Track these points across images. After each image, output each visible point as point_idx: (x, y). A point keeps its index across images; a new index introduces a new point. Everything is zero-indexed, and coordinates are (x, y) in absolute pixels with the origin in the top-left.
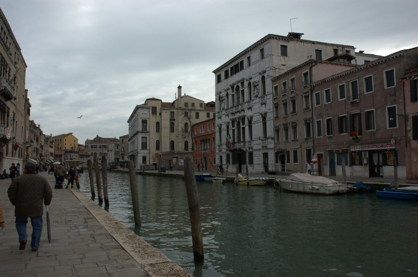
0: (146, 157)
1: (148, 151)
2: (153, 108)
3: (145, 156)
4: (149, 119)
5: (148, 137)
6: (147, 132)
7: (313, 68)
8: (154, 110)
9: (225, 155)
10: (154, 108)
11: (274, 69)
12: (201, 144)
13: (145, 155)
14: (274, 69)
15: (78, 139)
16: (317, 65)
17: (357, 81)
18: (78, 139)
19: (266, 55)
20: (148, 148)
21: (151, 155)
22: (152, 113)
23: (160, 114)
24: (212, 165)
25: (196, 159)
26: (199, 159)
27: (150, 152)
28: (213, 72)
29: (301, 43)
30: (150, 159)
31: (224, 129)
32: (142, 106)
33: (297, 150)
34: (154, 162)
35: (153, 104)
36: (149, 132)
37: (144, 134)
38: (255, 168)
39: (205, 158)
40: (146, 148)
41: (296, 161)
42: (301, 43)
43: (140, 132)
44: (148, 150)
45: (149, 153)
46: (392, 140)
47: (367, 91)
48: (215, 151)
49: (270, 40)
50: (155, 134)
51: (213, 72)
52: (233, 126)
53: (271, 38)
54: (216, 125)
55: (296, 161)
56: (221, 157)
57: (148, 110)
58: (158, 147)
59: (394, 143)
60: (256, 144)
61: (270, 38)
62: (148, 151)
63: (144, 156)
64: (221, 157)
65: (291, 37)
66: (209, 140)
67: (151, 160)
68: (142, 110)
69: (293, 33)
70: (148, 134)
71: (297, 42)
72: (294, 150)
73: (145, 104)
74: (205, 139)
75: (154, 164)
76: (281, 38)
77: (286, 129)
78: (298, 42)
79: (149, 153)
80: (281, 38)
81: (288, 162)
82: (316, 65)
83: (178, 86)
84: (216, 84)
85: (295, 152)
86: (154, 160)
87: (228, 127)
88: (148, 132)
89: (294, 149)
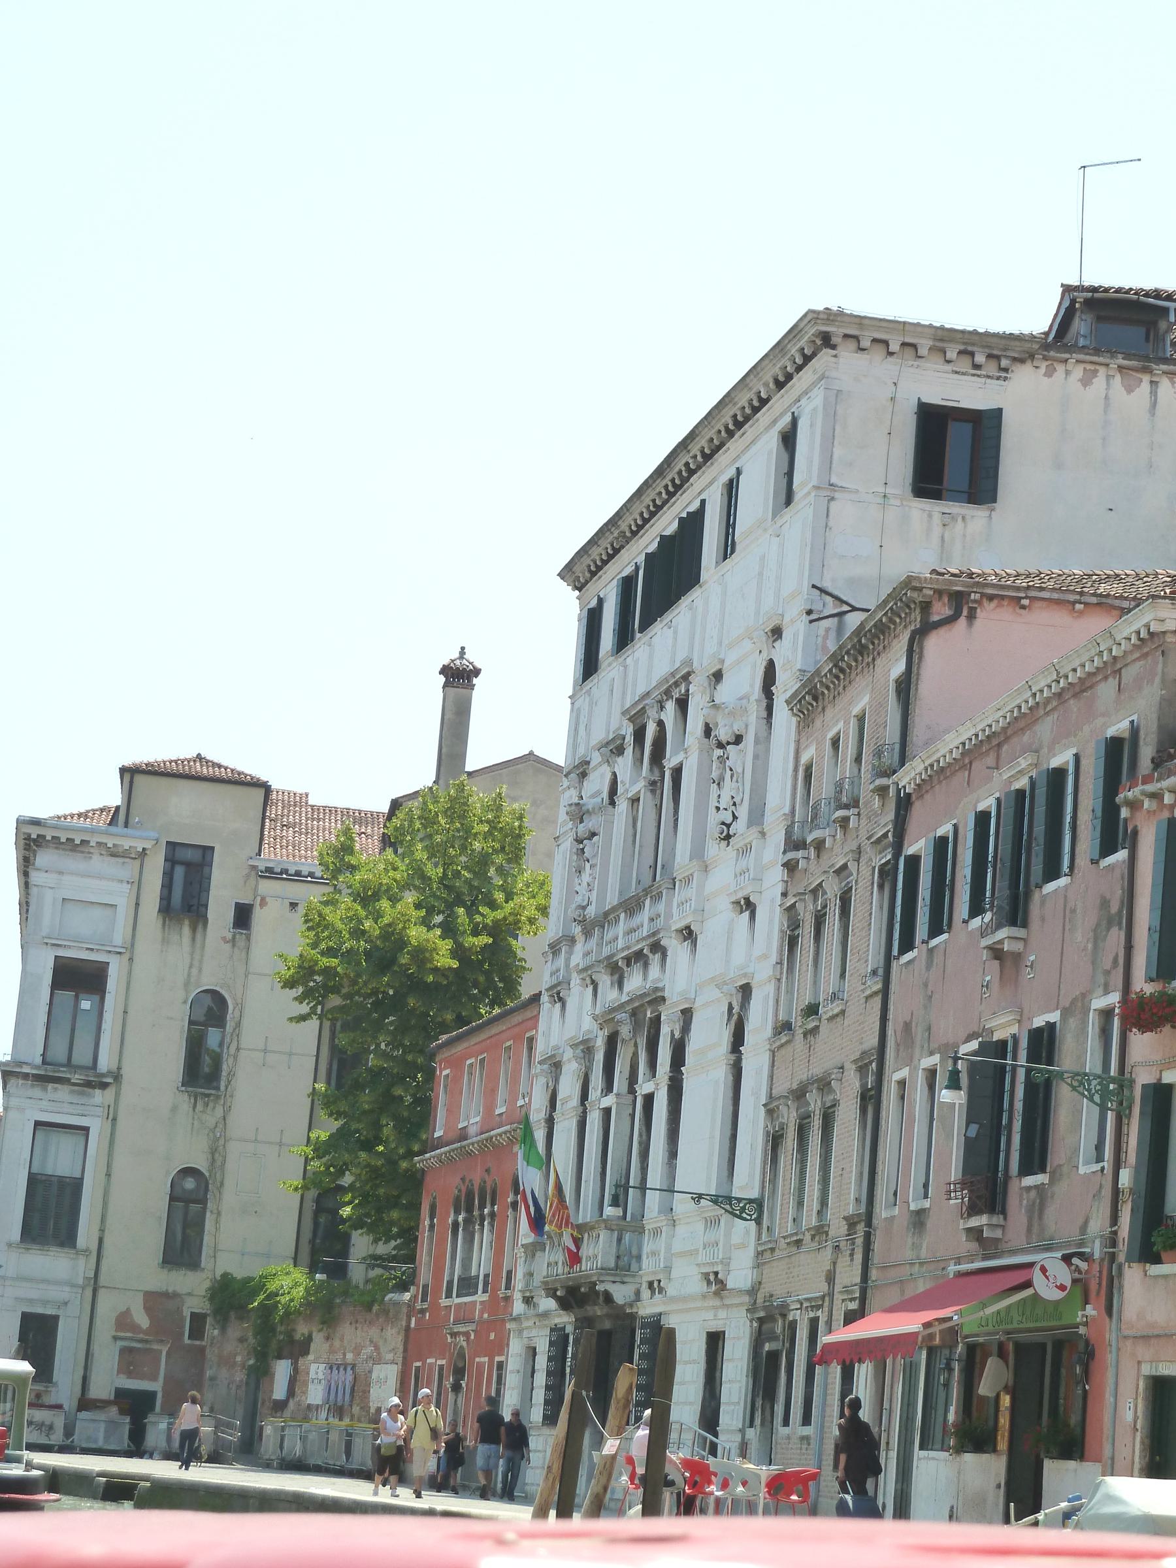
0: (55, 1319)
1: (83, 1268)
2: (181, 854)
3: (49, 1311)
4: (129, 951)
5: (96, 1126)
6: (88, 1084)
7: (934, 644)
8: (185, 886)
10: (189, 855)
11: (831, 608)
13: (45, 1303)
14: (831, 608)
16: (971, 617)
20: (86, 1234)
21: (108, 1307)
22: (166, 909)
23: (243, 916)
27: (103, 1280)
29: (1129, 390)
30: (96, 1347)
32: (66, 829)
34: (130, 1374)
35: (186, 814)
36: (117, 1077)
37: (62, 1093)
40: (66, 1238)
41: (806, 1420)
42: (1129, 390)
43: (26, 1076)
44: (87, 1251)
45: (95, 1284)
46: (1043, 1270)
49: (824, 358)
50: (174, 1109)
53: (834, 347)
54: (538, 1057)
55: (806, 1420)
57: (129, 870)
58: (182, 1245)
59: (1062, 1288)
61: (826, 340)
62: (82, 1261)
63: (39, 1310)
65: (1081, 326)
67: (107, 1358)
68: (71, 862)
69: (1094, 290)
70: (98, 1096)
71: (1086, 382)
73: (118, 817)
75: (121, 1394)
76: (924, 345)
78: (1100, 381)
79: (95, 1284)
80: (924, 345)
81: (786, 1423)
82: (962, 621)
83: (449, 655)
84: (575, 682)
86: (130, 1360)
88: (104, 1086)
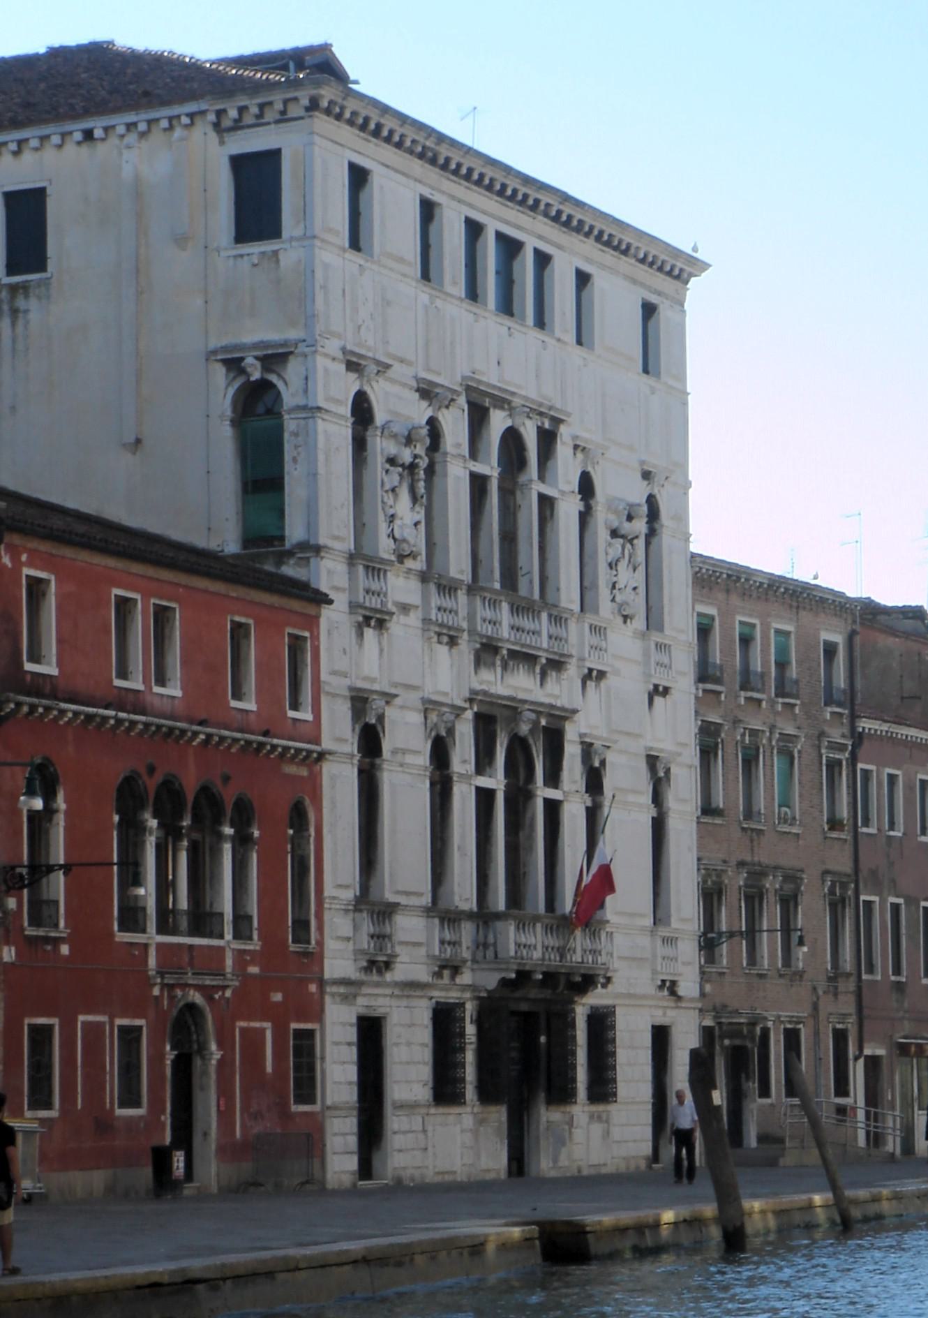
9: (424, 1016)
12: (131, 832)
15: (675, 268)
17: (546, 801)
18: (675, 268)
19: (583, 279)
24: (285, 1115)
25: (41, 1036)
26: (94, 1032)
28: (710, 266)
31: (404, 752)
33: (801, 1026)
38: (616, 1133)
39: (185, 1027)
47: (49, 1028)
48: (315, 958)
51: (710, 266)
52: (484, 761)
56: (370, 1034)
60: (634, 959)
64: (370, 1034)
66: (243, 814)
72: (789, 1026)
74: (190, 784)
77: (754, 899)
85: (792, 1038)
87: (440, 752)
89: (790, 1022)
